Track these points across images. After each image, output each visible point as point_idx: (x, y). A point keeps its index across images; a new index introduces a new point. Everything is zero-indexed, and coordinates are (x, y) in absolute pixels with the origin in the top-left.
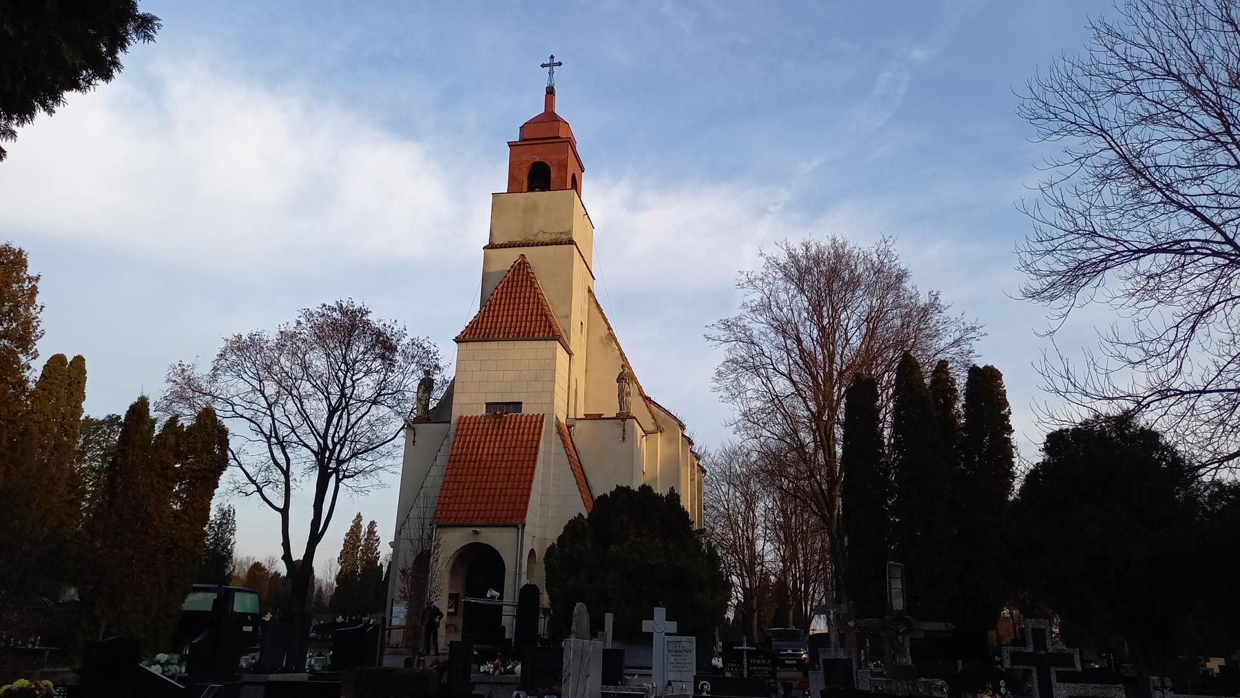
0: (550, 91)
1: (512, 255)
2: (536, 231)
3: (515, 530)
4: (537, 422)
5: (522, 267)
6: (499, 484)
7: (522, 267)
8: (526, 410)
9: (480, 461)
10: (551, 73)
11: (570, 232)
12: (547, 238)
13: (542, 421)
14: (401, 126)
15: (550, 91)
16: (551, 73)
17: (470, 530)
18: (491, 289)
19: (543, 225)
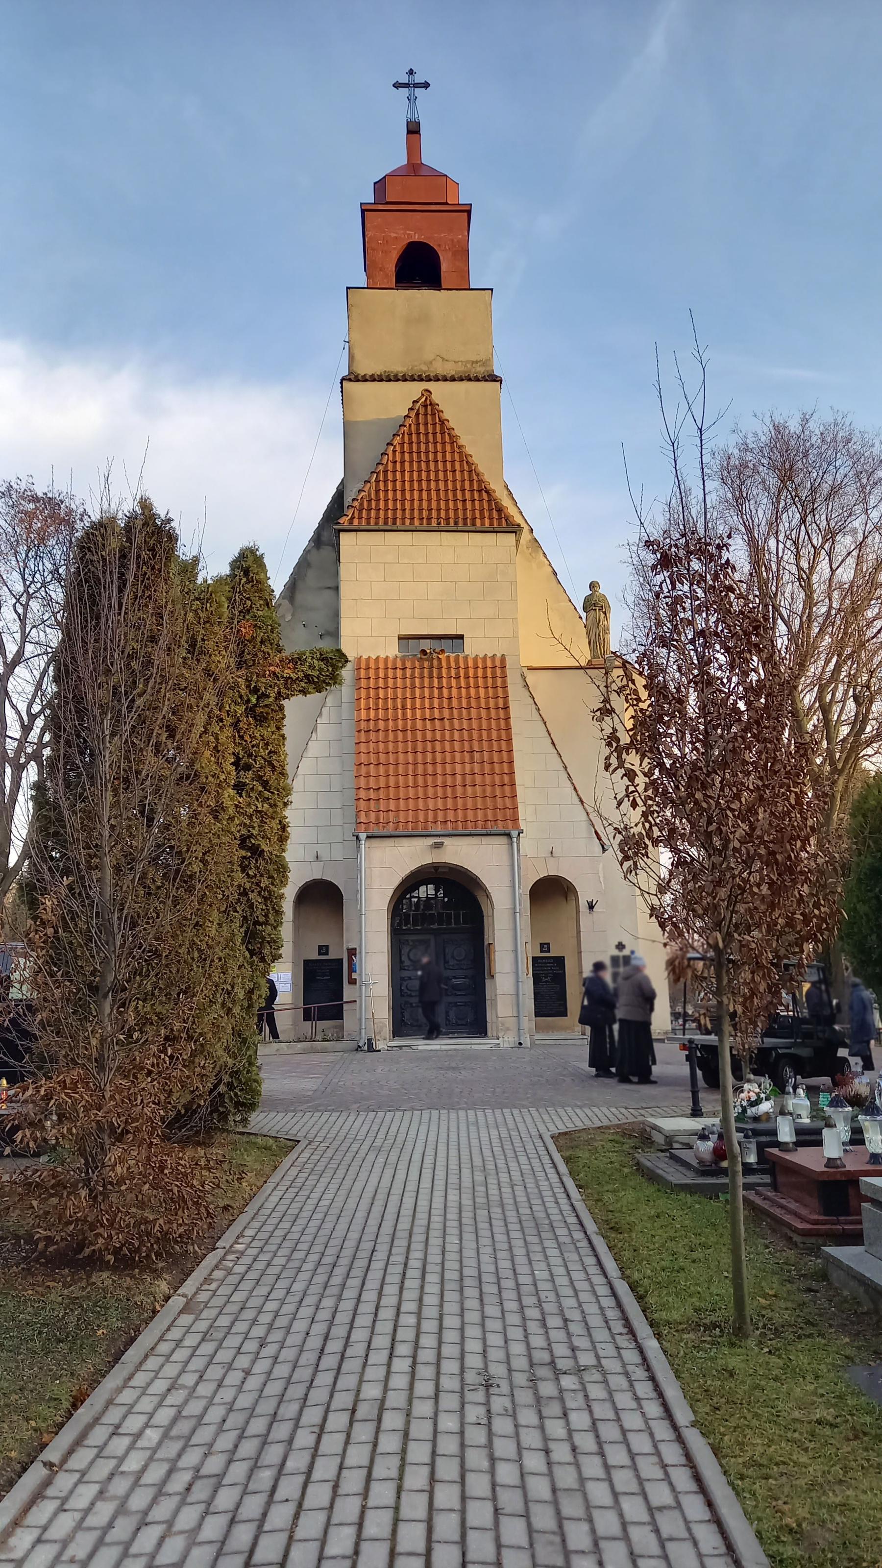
0: (413, 130)
1: (397, 400)
2: (431, 357)
3: (504, 840)
4: (495, 671)
5: (427, 409)
6: (431, 804)
7: (427, 409)
8: (473, 648)
9: (414, 730)
10: (412, 99)
11: (488, 362)
12: (449, 369)
13: (503, 667)
14: (31, 824)
15: (413, 130)
16: (412, 99)
17: (431, 841)
18: (364, 467)
19: (441, 348)
